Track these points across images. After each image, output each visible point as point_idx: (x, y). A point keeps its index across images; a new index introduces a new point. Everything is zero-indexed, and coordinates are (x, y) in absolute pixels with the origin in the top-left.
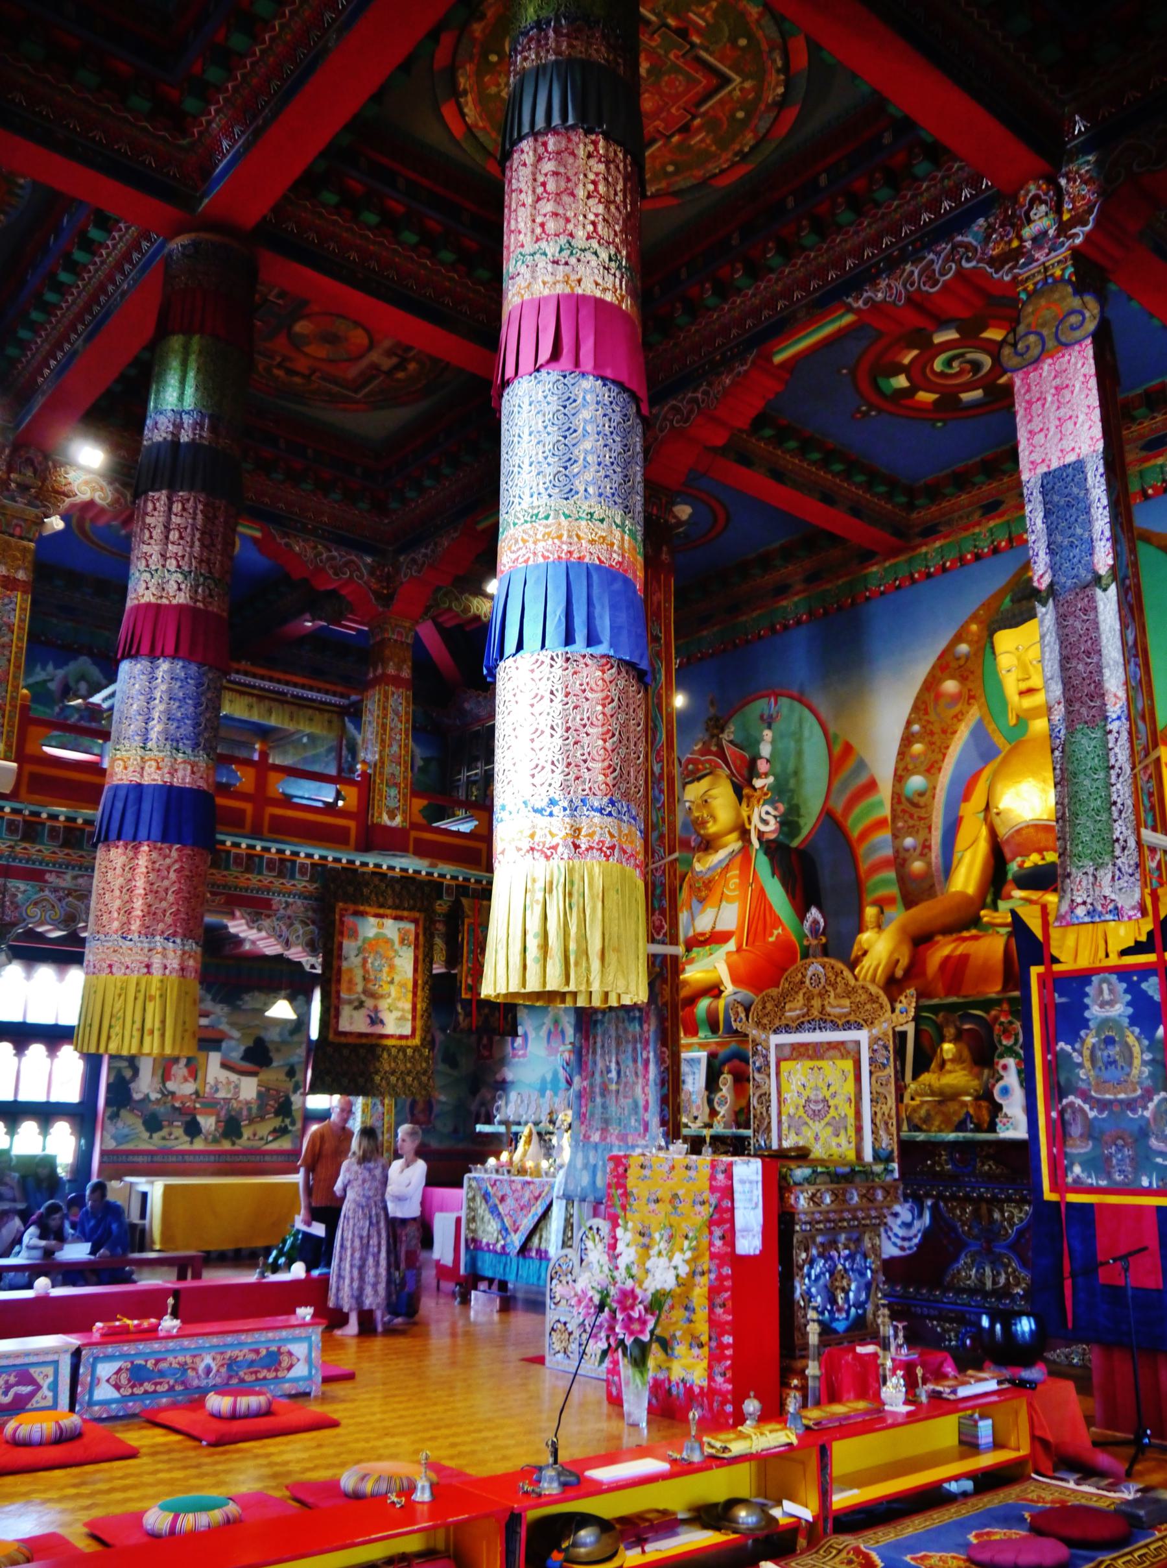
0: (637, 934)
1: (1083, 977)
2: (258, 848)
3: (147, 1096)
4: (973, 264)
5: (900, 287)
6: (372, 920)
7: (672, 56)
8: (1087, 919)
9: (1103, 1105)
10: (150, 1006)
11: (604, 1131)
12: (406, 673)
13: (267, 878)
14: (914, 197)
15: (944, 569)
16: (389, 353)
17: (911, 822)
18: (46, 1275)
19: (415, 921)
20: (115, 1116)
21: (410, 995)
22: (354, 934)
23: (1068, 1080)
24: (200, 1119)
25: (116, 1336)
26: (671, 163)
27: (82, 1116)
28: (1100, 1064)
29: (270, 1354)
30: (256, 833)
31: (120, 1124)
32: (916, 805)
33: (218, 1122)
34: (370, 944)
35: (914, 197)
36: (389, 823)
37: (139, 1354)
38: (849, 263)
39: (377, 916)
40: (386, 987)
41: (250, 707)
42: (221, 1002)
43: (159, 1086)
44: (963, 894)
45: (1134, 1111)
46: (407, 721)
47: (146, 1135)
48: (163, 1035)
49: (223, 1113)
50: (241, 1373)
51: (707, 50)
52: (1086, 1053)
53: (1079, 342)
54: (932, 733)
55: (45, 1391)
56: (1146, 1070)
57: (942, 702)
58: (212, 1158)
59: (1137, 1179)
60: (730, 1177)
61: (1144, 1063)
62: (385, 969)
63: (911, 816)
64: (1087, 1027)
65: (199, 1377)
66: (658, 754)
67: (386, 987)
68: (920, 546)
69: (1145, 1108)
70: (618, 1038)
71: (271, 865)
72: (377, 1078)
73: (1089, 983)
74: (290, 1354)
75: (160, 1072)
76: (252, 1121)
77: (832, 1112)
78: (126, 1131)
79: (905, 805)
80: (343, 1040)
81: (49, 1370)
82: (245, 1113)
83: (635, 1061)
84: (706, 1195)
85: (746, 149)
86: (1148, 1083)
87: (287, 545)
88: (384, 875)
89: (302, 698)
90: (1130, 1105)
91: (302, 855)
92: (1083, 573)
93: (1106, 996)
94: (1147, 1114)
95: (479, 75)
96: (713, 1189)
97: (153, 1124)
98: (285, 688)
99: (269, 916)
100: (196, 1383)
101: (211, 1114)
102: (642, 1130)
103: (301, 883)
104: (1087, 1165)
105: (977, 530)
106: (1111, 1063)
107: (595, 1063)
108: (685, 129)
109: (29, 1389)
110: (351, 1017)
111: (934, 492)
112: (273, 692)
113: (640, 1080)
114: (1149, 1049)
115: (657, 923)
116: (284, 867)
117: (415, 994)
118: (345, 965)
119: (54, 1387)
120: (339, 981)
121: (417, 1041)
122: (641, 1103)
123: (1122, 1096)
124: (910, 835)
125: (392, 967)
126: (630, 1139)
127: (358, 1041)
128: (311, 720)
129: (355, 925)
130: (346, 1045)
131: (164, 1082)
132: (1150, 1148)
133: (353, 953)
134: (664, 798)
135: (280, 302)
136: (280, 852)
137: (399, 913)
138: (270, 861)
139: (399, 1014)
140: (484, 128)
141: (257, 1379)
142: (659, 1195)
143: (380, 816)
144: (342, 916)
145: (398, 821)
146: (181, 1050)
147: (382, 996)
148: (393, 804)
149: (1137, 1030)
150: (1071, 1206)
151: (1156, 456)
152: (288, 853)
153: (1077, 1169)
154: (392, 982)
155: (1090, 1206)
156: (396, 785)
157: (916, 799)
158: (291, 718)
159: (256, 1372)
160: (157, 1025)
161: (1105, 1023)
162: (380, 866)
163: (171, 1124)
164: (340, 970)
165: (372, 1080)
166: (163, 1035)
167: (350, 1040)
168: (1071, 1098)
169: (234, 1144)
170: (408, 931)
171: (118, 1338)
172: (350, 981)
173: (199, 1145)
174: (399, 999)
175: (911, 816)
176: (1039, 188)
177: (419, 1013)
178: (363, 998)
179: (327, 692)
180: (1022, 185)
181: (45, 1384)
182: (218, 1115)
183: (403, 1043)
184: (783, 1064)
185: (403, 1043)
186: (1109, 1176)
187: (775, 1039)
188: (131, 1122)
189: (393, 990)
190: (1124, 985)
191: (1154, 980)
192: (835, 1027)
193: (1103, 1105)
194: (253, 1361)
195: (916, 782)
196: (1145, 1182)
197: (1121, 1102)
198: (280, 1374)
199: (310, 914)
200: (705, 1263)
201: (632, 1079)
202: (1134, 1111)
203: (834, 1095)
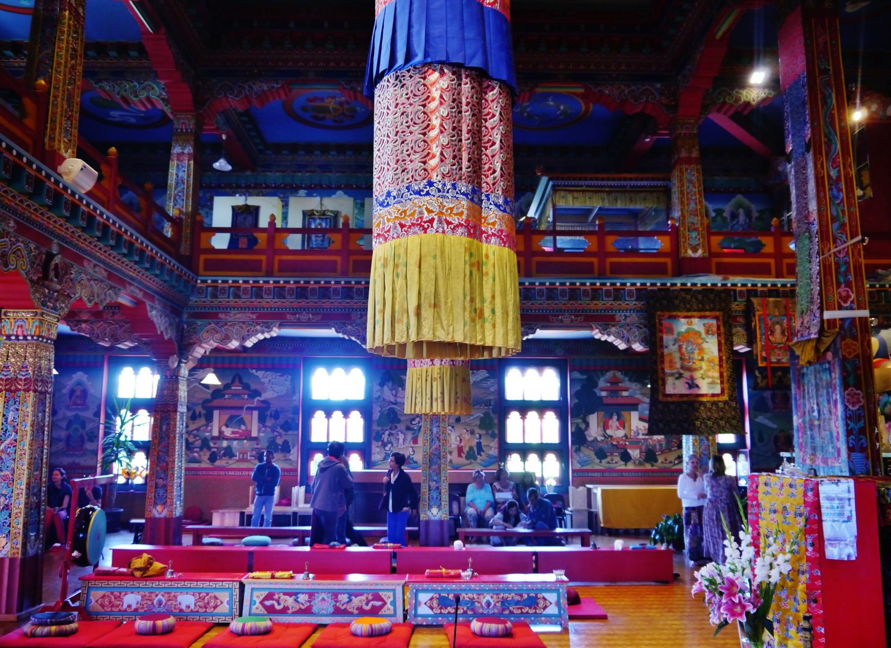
0: (446, 297)
2: (598, 284)
3: (596, 438)
6: (683, 320)
10: (434, 384)
11: (814, 454)
12: (695, 154)
13: (609, 302)
18: (457, 539)
19: (717, 318)
20: (578, 450)
21: (717, 367)
22: (671, 331)
24: (629, 451)
25: (437, 578)
27: (561, 450)
29: (529, 598)
30: (602, 275)
31: (581, 455)
33: (641, 452)
34: (683, 336)
36: (693, 255)
37: (443, 590)
39: (685, 317)
40: (697, 363)
41: (603, 199)
42: (634, 381)
43: (602, 433)
46: (700, 185)
47: (598, 461)
48: (443, 401)
49: (644, 447)
50: (511, 608)
55: (389, 605)
58: (640, 474)
60: (817, 494)
62: (696, 352)
65: (482, 607)
66: (834, 161)
67: (697, 363)
70: (817, 386)
71: (608, 293)
72: (698, 423)
74: (545, 599)
75: (602, 424)
76: (663, 452)
78: (585, 458)
80: (669, 399)
81: (391, 594)
82: (658, 447)
84: (802, 509)
87: (600, 91)
88: (690, 290)
89: (637, 187)
91: (628, 284)
97: (601, 455)
98: (625, 183)
99: (614, 326)
100: (481, 611)
101: (636, 448)
102: (836, 453)
103: (632, 303)
107: (805, 405)
109: (380, 603)
110: (674, 384)
112: (617, 187)
113: (833, 417)
115: (844, 294)
116: (618, 294)
117: (721, 366)
118: (666, 351)
119: (394, 603)
120: (663, 362)
121: (725, 398)
122: (835, 434)
125: (701, 350)
127: (680, 400)
128: (645, 199)
129: (670, 324)
130: (672, 403)
131: (605, 431)
133: (671, 343)
134: (843, 195)
136: (613, 284)
137: (702, 313)
138: (607, 291)
139: (710, 380)
141: (522, 613)
142: (776, 507)
143: (686, 252)
144: (660, 320)
145: (700, 253)
146: (455, 410)
147: (696, 369)
148: (694, 243)
152: (618, 284)
154: (702, 359)
156: (696, 229)
158: (631, 201)
159: (521, 609)
160: (439, 395)
162: (685, 285)
163: (612, 454)
164: (662, 355)
165: (694, 425)
166: (443, 401)
167: (674, 399)
169: (653, 465)
170: (712, 325)
171: (433, 580)
172: (671, 361)
173: (630, 466)
174: (709, 370)
177: (725, 379)
178: (682, 371)
179: (653, 179)
181: (389, 602)
182: (641, 449)
183: (716, 399)
185: (716, 399)
188: (588, 453)
189: (704, 365)
194: (518, 601)
198: (538, 611)
199: (642, 321)
200: (805, 566)
201: (827, 416)
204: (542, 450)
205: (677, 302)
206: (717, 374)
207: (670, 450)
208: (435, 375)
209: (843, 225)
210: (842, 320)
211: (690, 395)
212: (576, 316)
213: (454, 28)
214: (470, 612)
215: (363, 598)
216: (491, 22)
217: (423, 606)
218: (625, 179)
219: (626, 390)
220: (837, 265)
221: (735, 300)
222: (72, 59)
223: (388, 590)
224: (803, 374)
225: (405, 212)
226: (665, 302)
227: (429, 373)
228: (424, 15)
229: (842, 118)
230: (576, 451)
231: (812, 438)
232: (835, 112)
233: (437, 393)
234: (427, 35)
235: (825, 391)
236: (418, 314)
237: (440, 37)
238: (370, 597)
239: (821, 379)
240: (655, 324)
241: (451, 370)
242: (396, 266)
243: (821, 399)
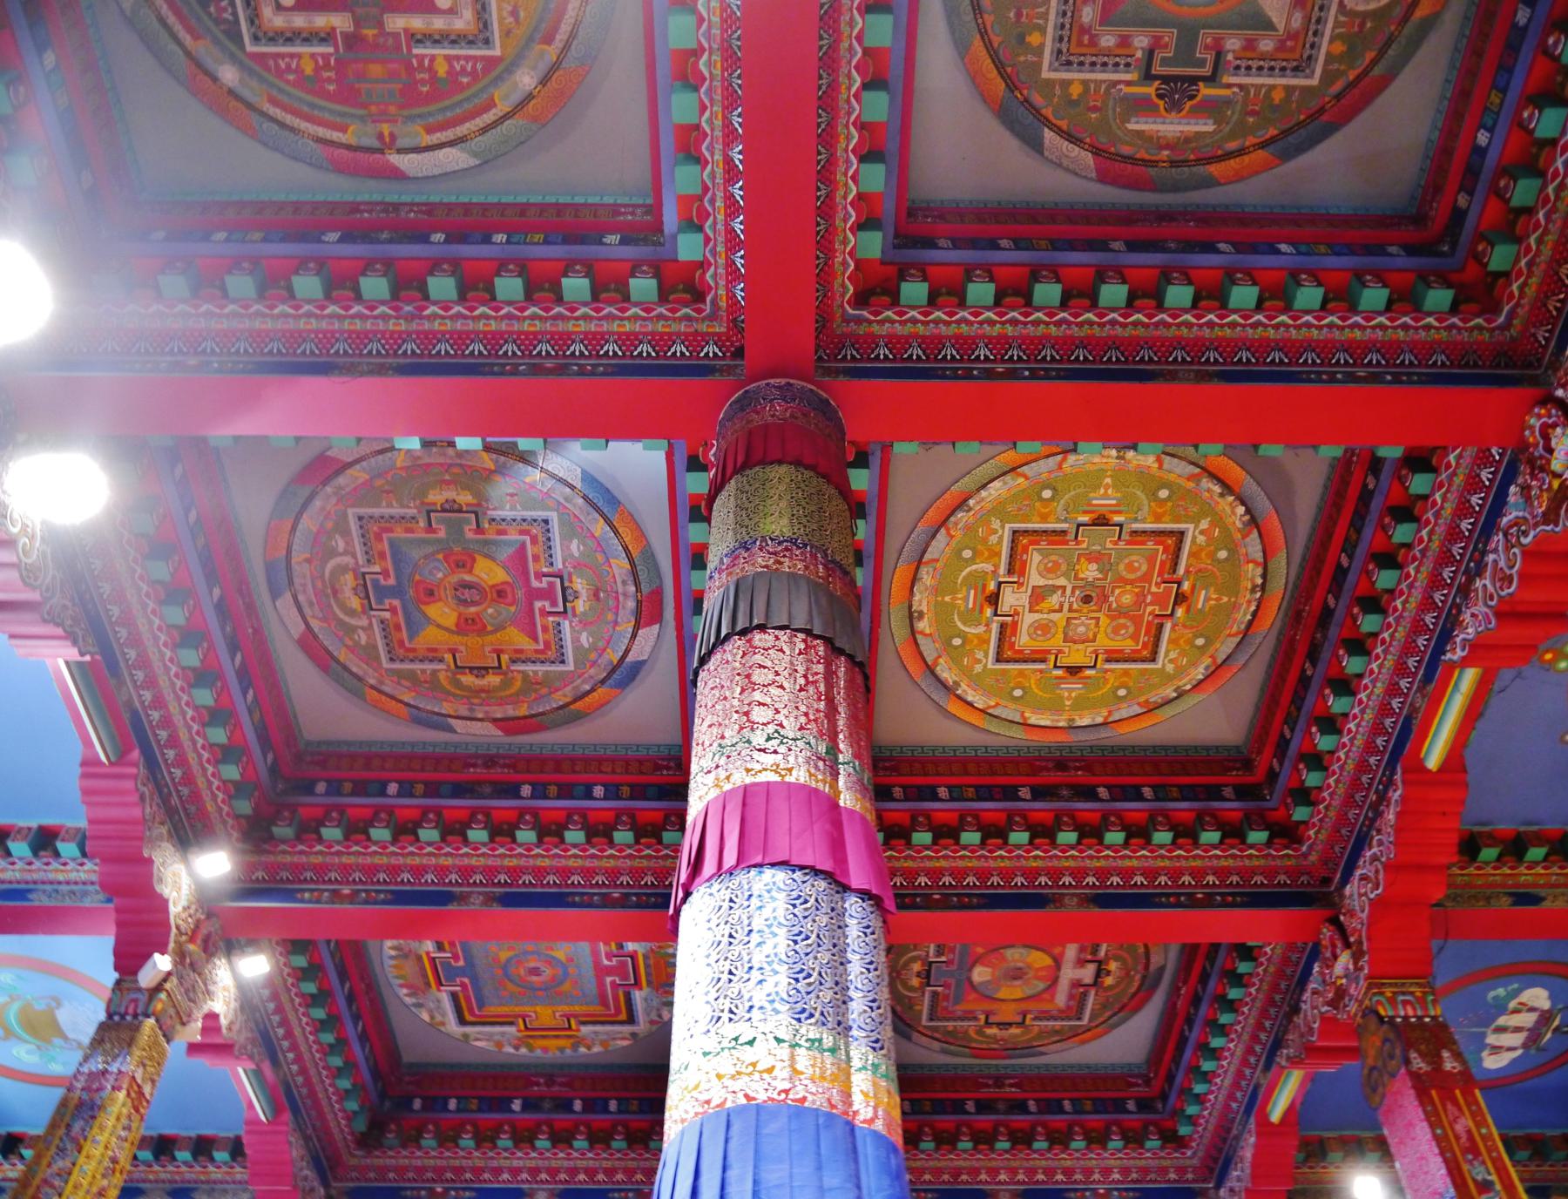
4: (1532, 534)
7: (1109, 545)
14: (1437, 515)
16: (1081, 963)
26: (1196, 637)
35: (1437, 515)
51: (1136, 520)
85: (1259, 581)
95: (956, 661)
108: (1180, 599)
135: (943, 959)
140: (997, 704)
176: (1539, 416)
180: (1523, 426)
213: (805, 1169)
216: (869, 1153)
222: (104, 1176)
228: (752, 1146)
234: (756, 1182)
237: (777, 1186)
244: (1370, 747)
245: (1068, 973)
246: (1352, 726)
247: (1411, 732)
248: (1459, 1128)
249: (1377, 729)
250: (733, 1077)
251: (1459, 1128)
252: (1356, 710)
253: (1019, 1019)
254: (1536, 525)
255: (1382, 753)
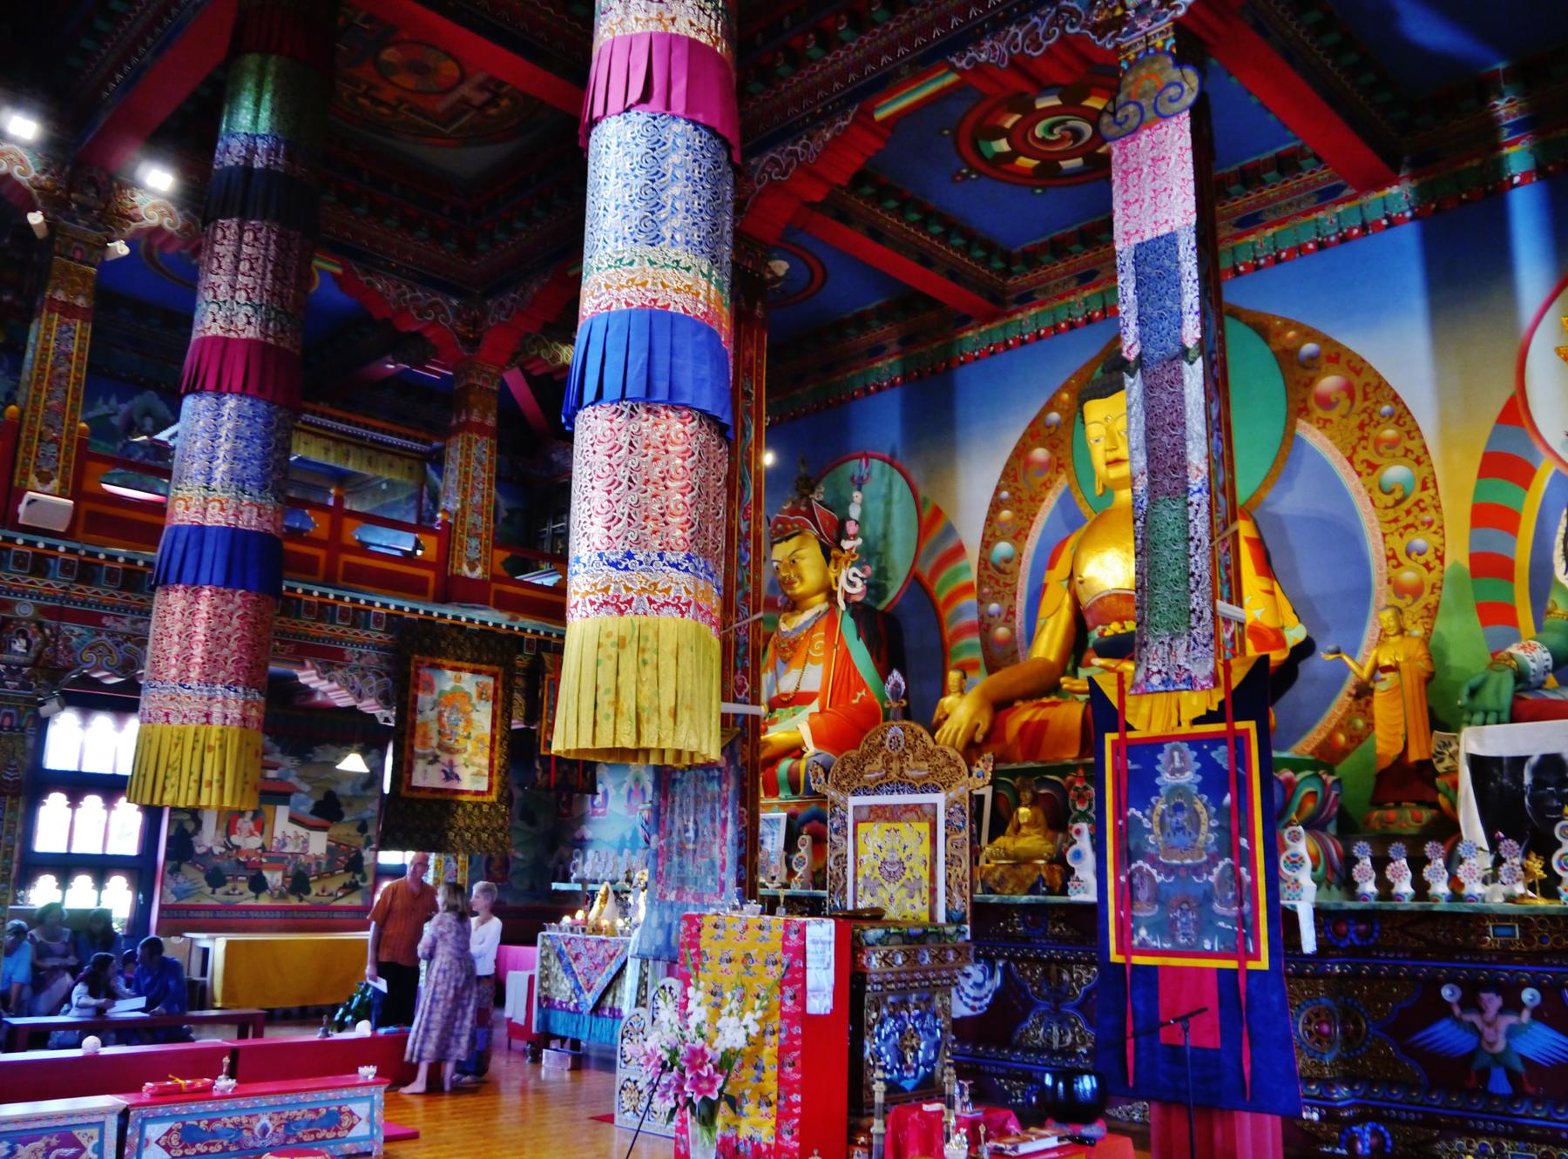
1: (1154, 745)
3: (210, 850)
4: (1077, 29)
5: (1004, 50)
6: (449, 673)
8: (1161, 688)
9: (1169, 870)
10: (209, 757)
12: (491, 421)
15: (1038, 337)
17: (997, 588)
19: (494, 675)
20: (175, 870)
21: (487, 751)
22: (430, 687)
23: (1138, 846)
24: (266, 874)
27: (139, 869)
28: (1169, 830)
30: (329, 581)
31: (180, 879)
32: (1002, 571)
33: (285, 877)
36: (469, 574)
38: (955, 21)
40: (462, 741)
41: (327, 450)
42: (291, 754)
43: (222, 840)
44: (1044, 661)
45: (1199, 876)
46: (491, 471)
48: (222, 787)
50: (300, 1134)
52: (1156, 819)
53: (1176, 114)
54: (1020, 500)
56: (1212, 837)
57: (1031, 469)
58: (278, 914)
59: (1199, 941)
60: (803, 937)
61: (1211, 830)
62: (462, 724)
63: (997, 583)
64: (1158, 794)
68: (1016, 312)
69: (1210, 873)
70: (697, 797)
72: (451, 835)
73: (1161, 750)
74: (351, 1113)
75: (224, 825)
76: (320, 876)
77: (907, 872)
78: (187, 886)
79: (992, 571)
80: (416, 795)
81: (95, 1132)
82: (314, 868)
83: (713, 820)
86: (1214, 849)
89: (381, 442)
90: (1196, 870)
92: (1171, 345)
93: (1177, 764)
94: (1212, 879)
96: (785, 949)
97: (216, 879)
98: (364, 432)
99: (341, 667)
101: (277, 869)
103: (376, 634)
104: (1154, 928)
105: (1072, 299)
106: (1180, 829)
111: (1031, 259)
112: (353, 435)
113: (718, 840)
114: (1216, 816)
116: (358, 617)
117: (492, 749)
118: (419, 718)
120: (413, 735)
121: (493, 798)
122: (718, 863)
123: (1188, 861)
124: (995, 600)
125: (469, 722)
126: (706, 899)
127: (431, 796)
128: (391, 466)
130: (419, 801)
131: (228, 835)
132: (1213, 912)
133: (428, 707)
134: (750, 557)
137: (478, 667)
138: (344, 610)
139: (475, 769)
141: (316, 1139)
143: (460, 567)
144: (418, 668)
145: (478, 573)
147: (458, 751)
148: (474, 555)
149: (1205, 797)
150: (1135, 967)
151: (1249, 234)
153: (1143, 932)
154: (468, 737)
155: (1155, 967)
156: (479, 536)
157: (1003, 565)
160: (216, 777)
161: (1176, 790)
163: (235, 879)
166: (222, 787)
168: (1140, 863)
169: (301, 899)
172: (425, 735)
173: (264, 900)
175: (997, 583)
177: (496, 769)
178: (438, 752)
179: (408, 438)
182: (285, 871)
183: (479, 799)
184: (861, 826)
185: (479, 799)
186: (1173, 938)
187: (853, 801)
188: (193, 876)
189: (470, 745)
190: (1195, 753)
191: (1223, 749)
192: (913, 789)
193: (1169, 870)
194: (312, 1121)
195: (1003, 548)
196: (1207, 946)
197: (1188, 867)
200: (776, 1022)
201: (709, 838)
202: (1199, 876)
203: (909, 857)
204: (101, 867)
205: (443, 644)
206: (485, 762)
207: (332, 874)
208: (213, 742)
209: (747, 595)
210: (736, 715)
211: (446, 790)
212: (282, 642)
214: (233, 1148)
215: (40, 1144)
217: (363, 1116)
218: (366, 427)
219: (275, 768)
220: (737, 643)
221: (521, 652)
223: (90, 1125)
224: (675, 781)
225: (655, 585)
226: (427, 641)
227: (201, 738)
229: (758, 461)
230: (171, 872)
231: (681, 866)
232: (752, 449)
233: (211, 771)
235: (708, 807)
236: (675, 714)
238: (54, 1141)
239: (704, 790)
240: (408, 674)
241: (241, 736)
242: (641, 650)
243: (1427, 872)
244: (841, 76)
245: (466, 90)
246: (842, 54)
247: (885, 85)
248: (747, 354)
249: (858, 66)
250: (677, 291)
251: (747, 354)
252: (854, 45)
253: (394, 103)
254: (1083, 27)
255: (848, 85)
